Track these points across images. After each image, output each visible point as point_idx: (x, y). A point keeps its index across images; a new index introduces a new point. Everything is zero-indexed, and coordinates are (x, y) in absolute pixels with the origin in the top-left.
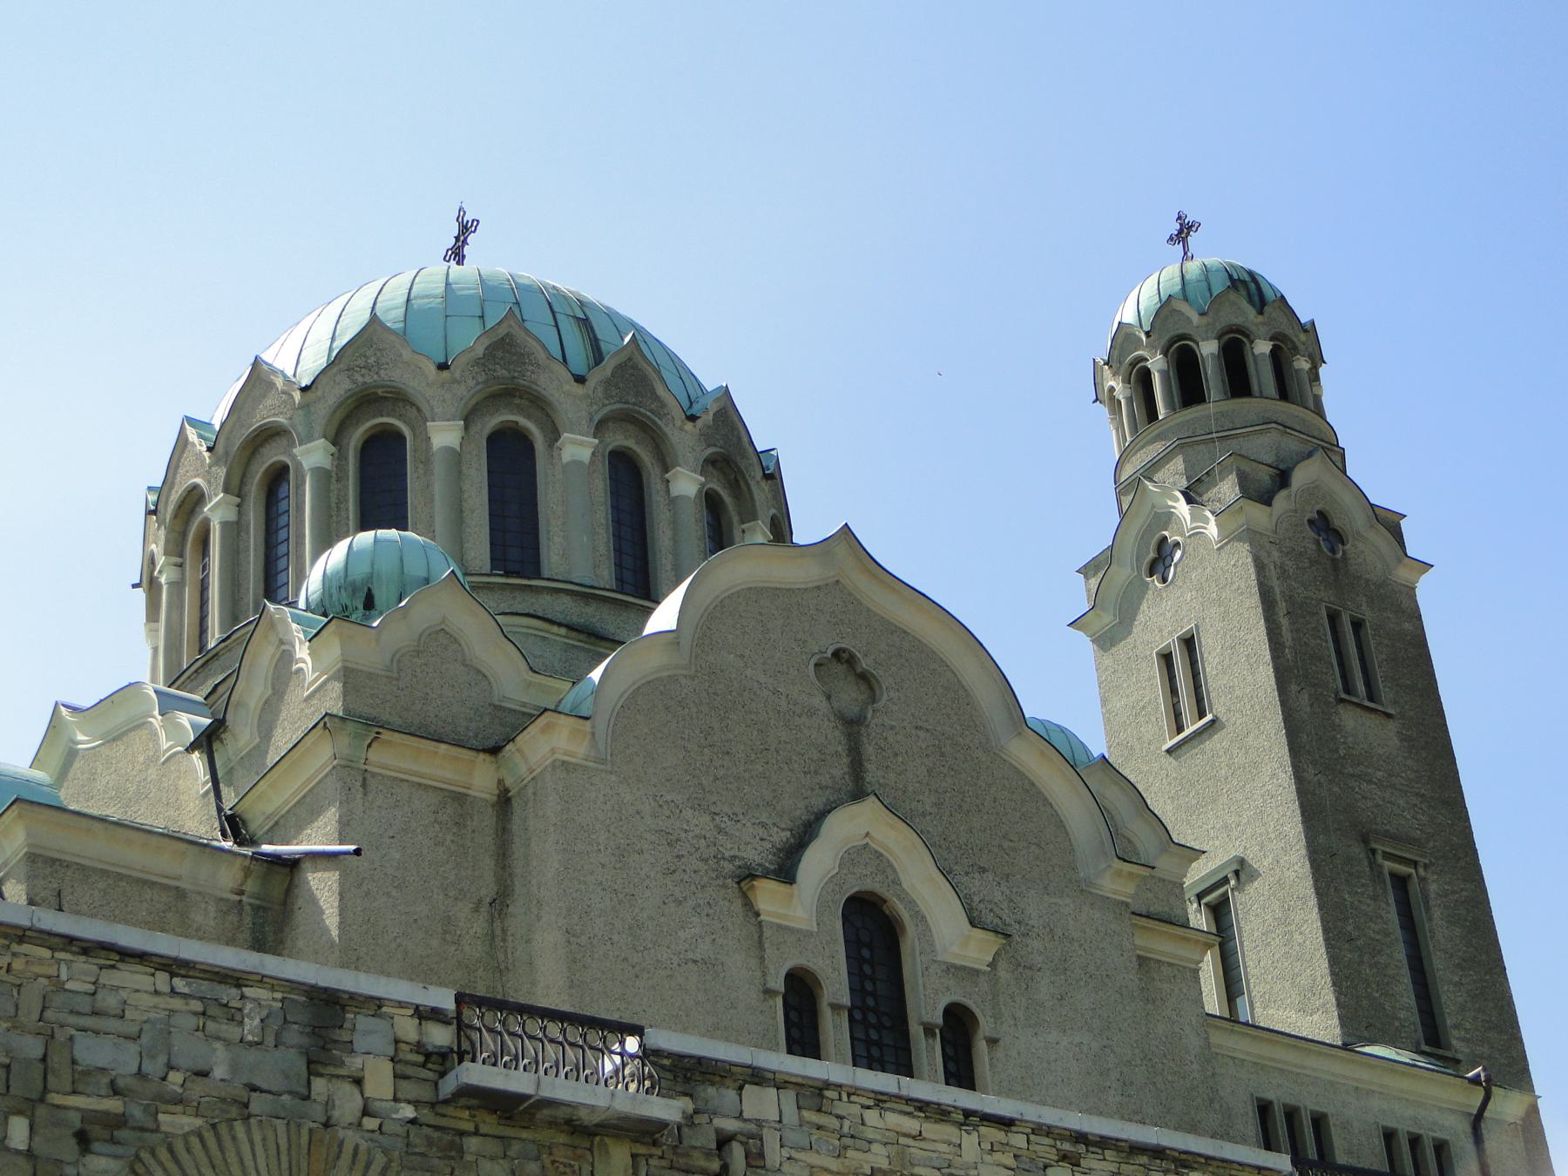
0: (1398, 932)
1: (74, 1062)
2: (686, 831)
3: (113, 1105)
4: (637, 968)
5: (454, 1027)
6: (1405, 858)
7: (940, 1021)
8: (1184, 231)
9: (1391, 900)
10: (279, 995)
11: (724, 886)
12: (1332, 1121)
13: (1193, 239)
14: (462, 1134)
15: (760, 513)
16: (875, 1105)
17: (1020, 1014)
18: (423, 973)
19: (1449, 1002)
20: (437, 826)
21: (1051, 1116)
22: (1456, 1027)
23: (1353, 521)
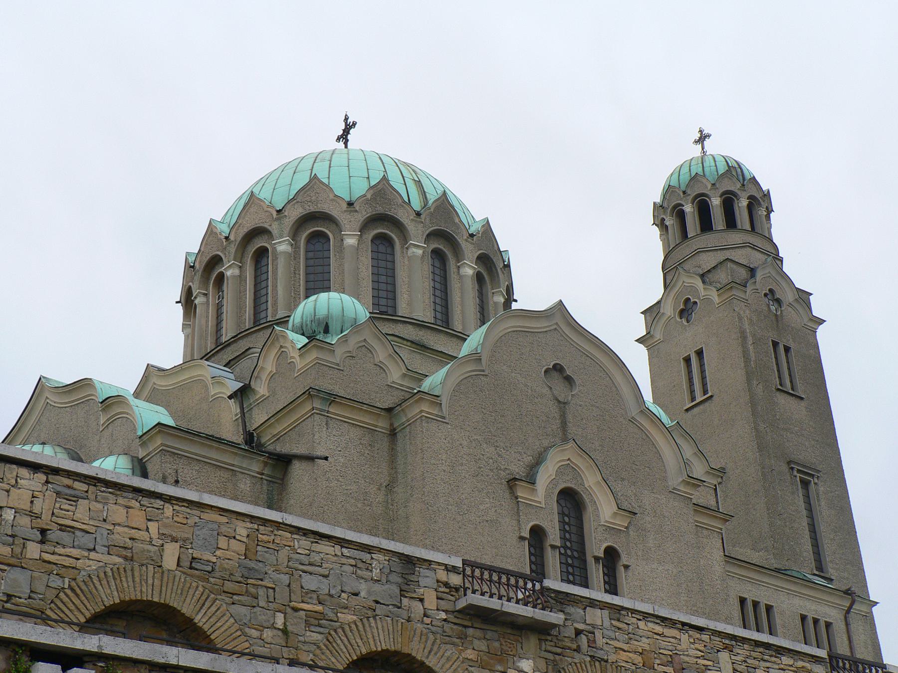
0: (805, 512)
1: (302, 587)
2: (483, 455)
3: (319, 608)
4: (460, 524)
5: (461, 575)
6: (809, 473)
7: (602, 556)
8: (702, 138)
9: (801, 495)
10: (387, 558)
11: (501, 484)
12: (775, 610)
13: (707, 142)
14: (188, 549)
15: (502, 285)
16: (644, 619)
17: (640, 553)
18: (451, 552)
19: (828, 549)
20: (361, 446)
21: (721, 627)
22: (831, 562)
23: (788, 297)
